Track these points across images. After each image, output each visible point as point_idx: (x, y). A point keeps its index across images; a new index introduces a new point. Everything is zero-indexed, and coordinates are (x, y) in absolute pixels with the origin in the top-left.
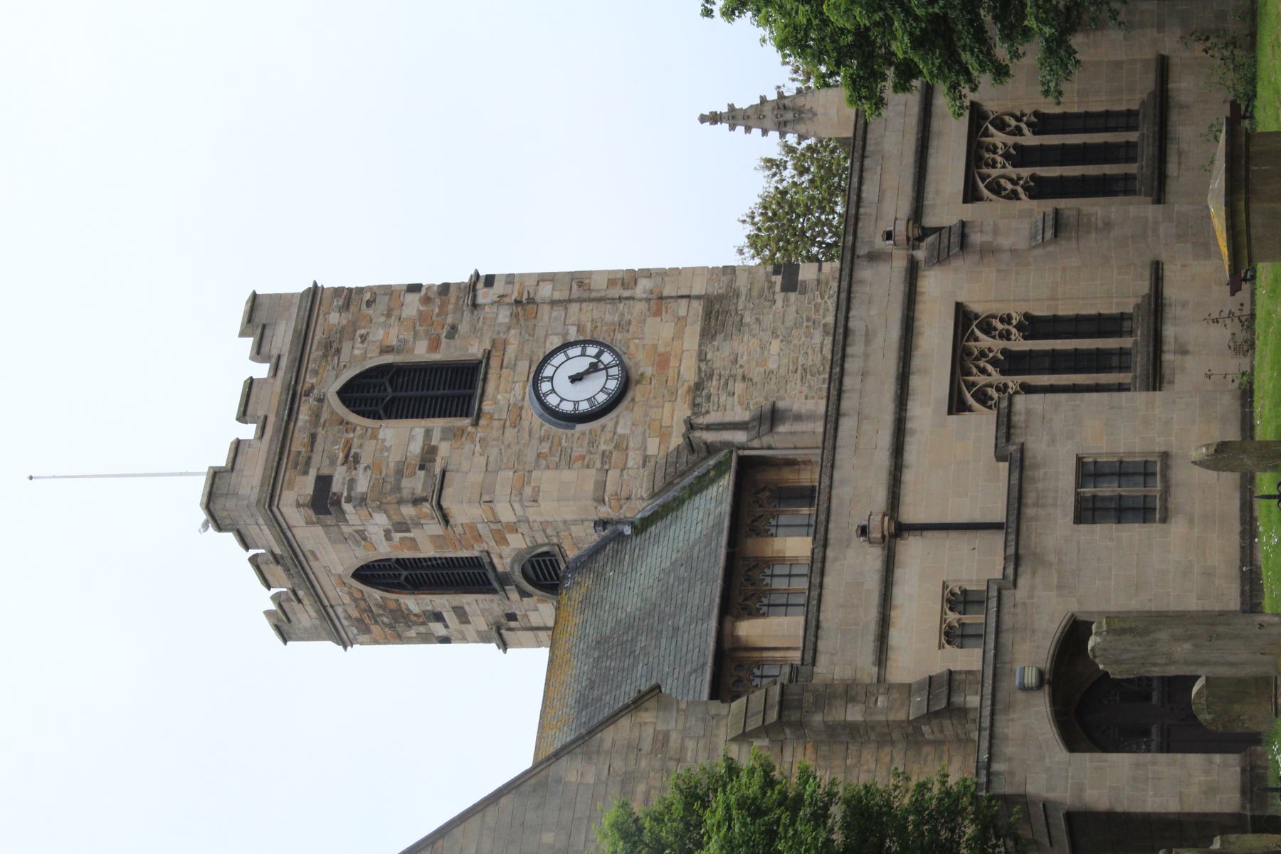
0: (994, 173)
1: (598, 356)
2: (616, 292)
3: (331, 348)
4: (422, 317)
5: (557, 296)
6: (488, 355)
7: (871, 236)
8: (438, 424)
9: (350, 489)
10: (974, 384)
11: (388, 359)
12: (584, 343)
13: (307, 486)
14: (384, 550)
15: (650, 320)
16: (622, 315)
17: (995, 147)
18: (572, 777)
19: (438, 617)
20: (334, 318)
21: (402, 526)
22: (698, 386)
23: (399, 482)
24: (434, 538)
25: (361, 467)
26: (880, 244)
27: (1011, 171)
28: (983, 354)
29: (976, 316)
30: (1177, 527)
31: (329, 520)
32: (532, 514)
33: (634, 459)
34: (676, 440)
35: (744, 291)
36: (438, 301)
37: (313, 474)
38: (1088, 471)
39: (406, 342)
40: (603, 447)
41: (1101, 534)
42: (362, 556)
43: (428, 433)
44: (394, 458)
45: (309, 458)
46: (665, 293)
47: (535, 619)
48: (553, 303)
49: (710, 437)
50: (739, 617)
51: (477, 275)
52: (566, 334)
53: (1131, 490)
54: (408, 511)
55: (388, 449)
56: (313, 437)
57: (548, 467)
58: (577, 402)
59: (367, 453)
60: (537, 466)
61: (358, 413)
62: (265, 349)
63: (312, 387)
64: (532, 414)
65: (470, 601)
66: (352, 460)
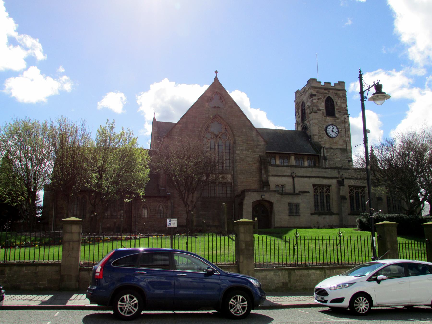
0: (354, 190)
1: (332, 127)
2: (347, 135)
3: (336, 94)
4: (342, 107)
5: (346, 127)
6: (336, 117)
7: (342, 172)
8: (325, 111)
9: (314, 99)
10: (318, 188)
11: (335, 103)
12: (338, 131)
13: (314, 93)
14: (306, 105)
15: (342, 141)
16: (343, 136)
17: (359, 190)
18: (254, 133)
19: (298, 114)
20: (341, 95)
21: (309, 107)
22: (332, 148)
23: (315, 106)
24: (308, 112)
25: (318, 101)
26: (341, 173)
27: (354, 192)
28: (323, 189)
29: (330, 188)
30: (288, 218)
31: (309, 97)
32: (311, 126)
33: (320, 140)
34: (323, 146)
35: (348, 154)
36: (344, 109)
37: (316, 94)
38: (297, 205)
39: (338, 105)
40: (322, 135)
41: (287, 207)
42: (305, 102)
43: (323, 110)
44: (319, 105)
45: (318, 93)
46: (347, 143)
47: (299, 128)
48: (345, 126)
49: (322, 150)
50: (294, 156)
51: (349, 115)
52: (340, 128)
53: (295, 211)
54: (311, 108)
55: (320, 104)
56: (322, 93)
57: (318, 127)
58: (329, 131)
59: (319, 101)
60: (318, 126)
61: (326, 99)
62: (336, 85)
63: (330, 92)
64: (326, 125)
65: (300, 119)
66: (318, 99)
